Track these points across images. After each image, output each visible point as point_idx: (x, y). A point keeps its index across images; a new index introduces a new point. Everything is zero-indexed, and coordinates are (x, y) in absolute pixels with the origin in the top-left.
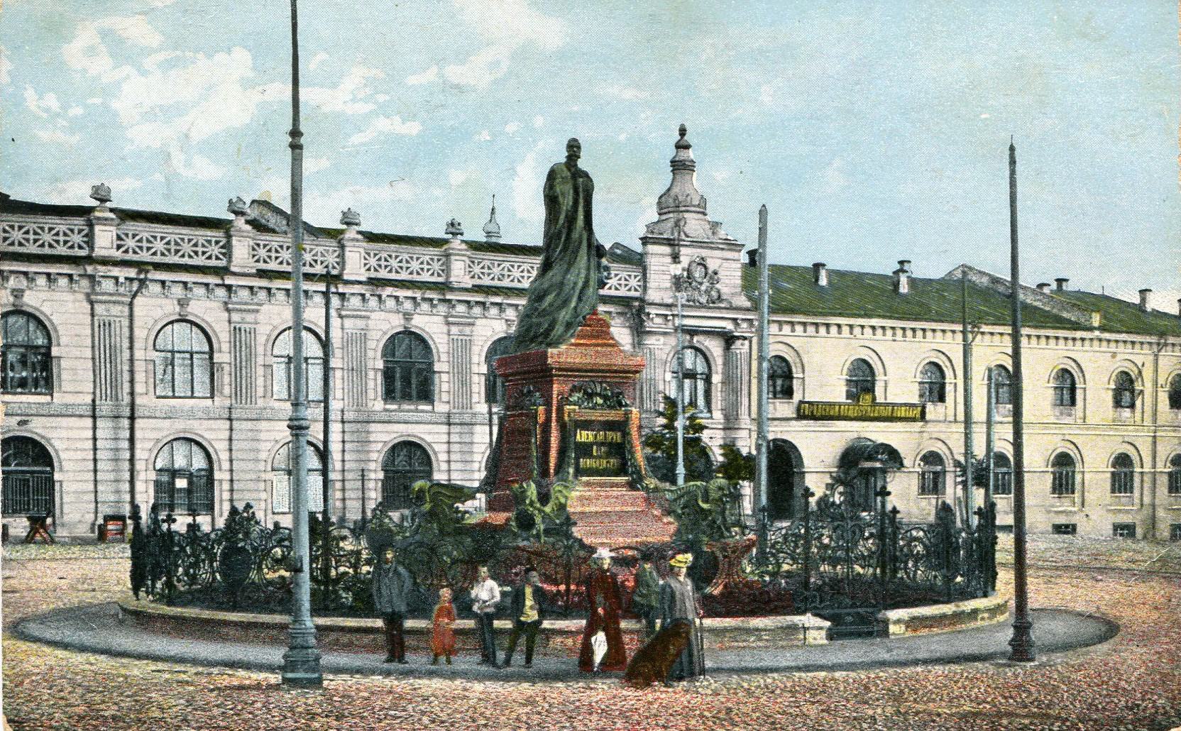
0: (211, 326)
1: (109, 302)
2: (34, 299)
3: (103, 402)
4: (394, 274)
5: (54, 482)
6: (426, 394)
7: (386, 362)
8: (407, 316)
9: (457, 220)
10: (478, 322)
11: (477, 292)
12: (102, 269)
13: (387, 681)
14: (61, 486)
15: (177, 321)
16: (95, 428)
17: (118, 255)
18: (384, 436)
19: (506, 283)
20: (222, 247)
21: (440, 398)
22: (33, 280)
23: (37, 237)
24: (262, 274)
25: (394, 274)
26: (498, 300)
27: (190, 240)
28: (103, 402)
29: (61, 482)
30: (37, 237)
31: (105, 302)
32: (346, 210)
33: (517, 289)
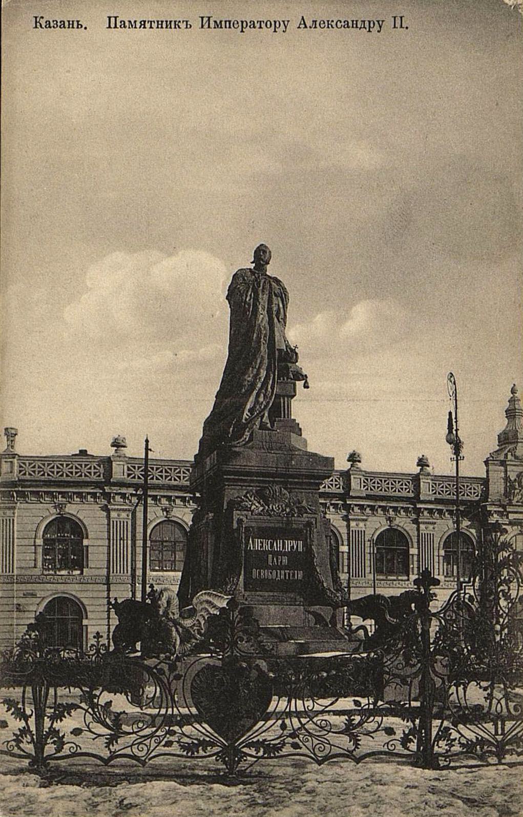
0: (408, 533)
1: (120, 510)
2: (71, 509)
3: (354, 578)
4: (173, 481)
5: (83, 626)
6: (80, 564)
7: (445, 551)
8: (60, 507)
9: (358, 451)
10: (370, 519)
11: (368, 499)
12: (115, 489)
13: (229, 788)
14: (87, 629)
15: (519, 534)
16: (109, 590)
17: (129, 480)
18: (47, 592)
19: (391, 493)
20: (142, 471)
21: (343, 570)
22: (85, 497)
23: (89, 471)
24: (368, 497)
25: (136, 479)
26: (383, 504)
27: (157, 469)
28: (354, 578)
29: (86, 626)
30: (89, 471)
31: (118, 510)
32: (421, 457)
33: (65, 482)
